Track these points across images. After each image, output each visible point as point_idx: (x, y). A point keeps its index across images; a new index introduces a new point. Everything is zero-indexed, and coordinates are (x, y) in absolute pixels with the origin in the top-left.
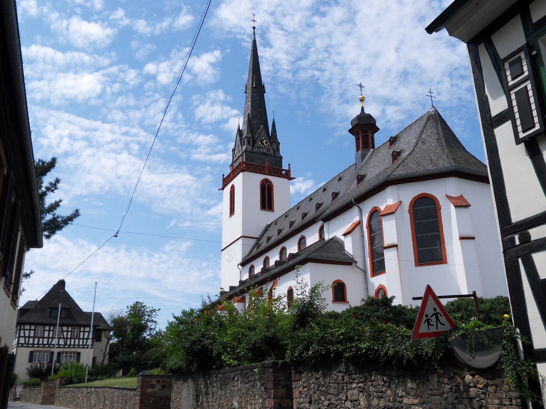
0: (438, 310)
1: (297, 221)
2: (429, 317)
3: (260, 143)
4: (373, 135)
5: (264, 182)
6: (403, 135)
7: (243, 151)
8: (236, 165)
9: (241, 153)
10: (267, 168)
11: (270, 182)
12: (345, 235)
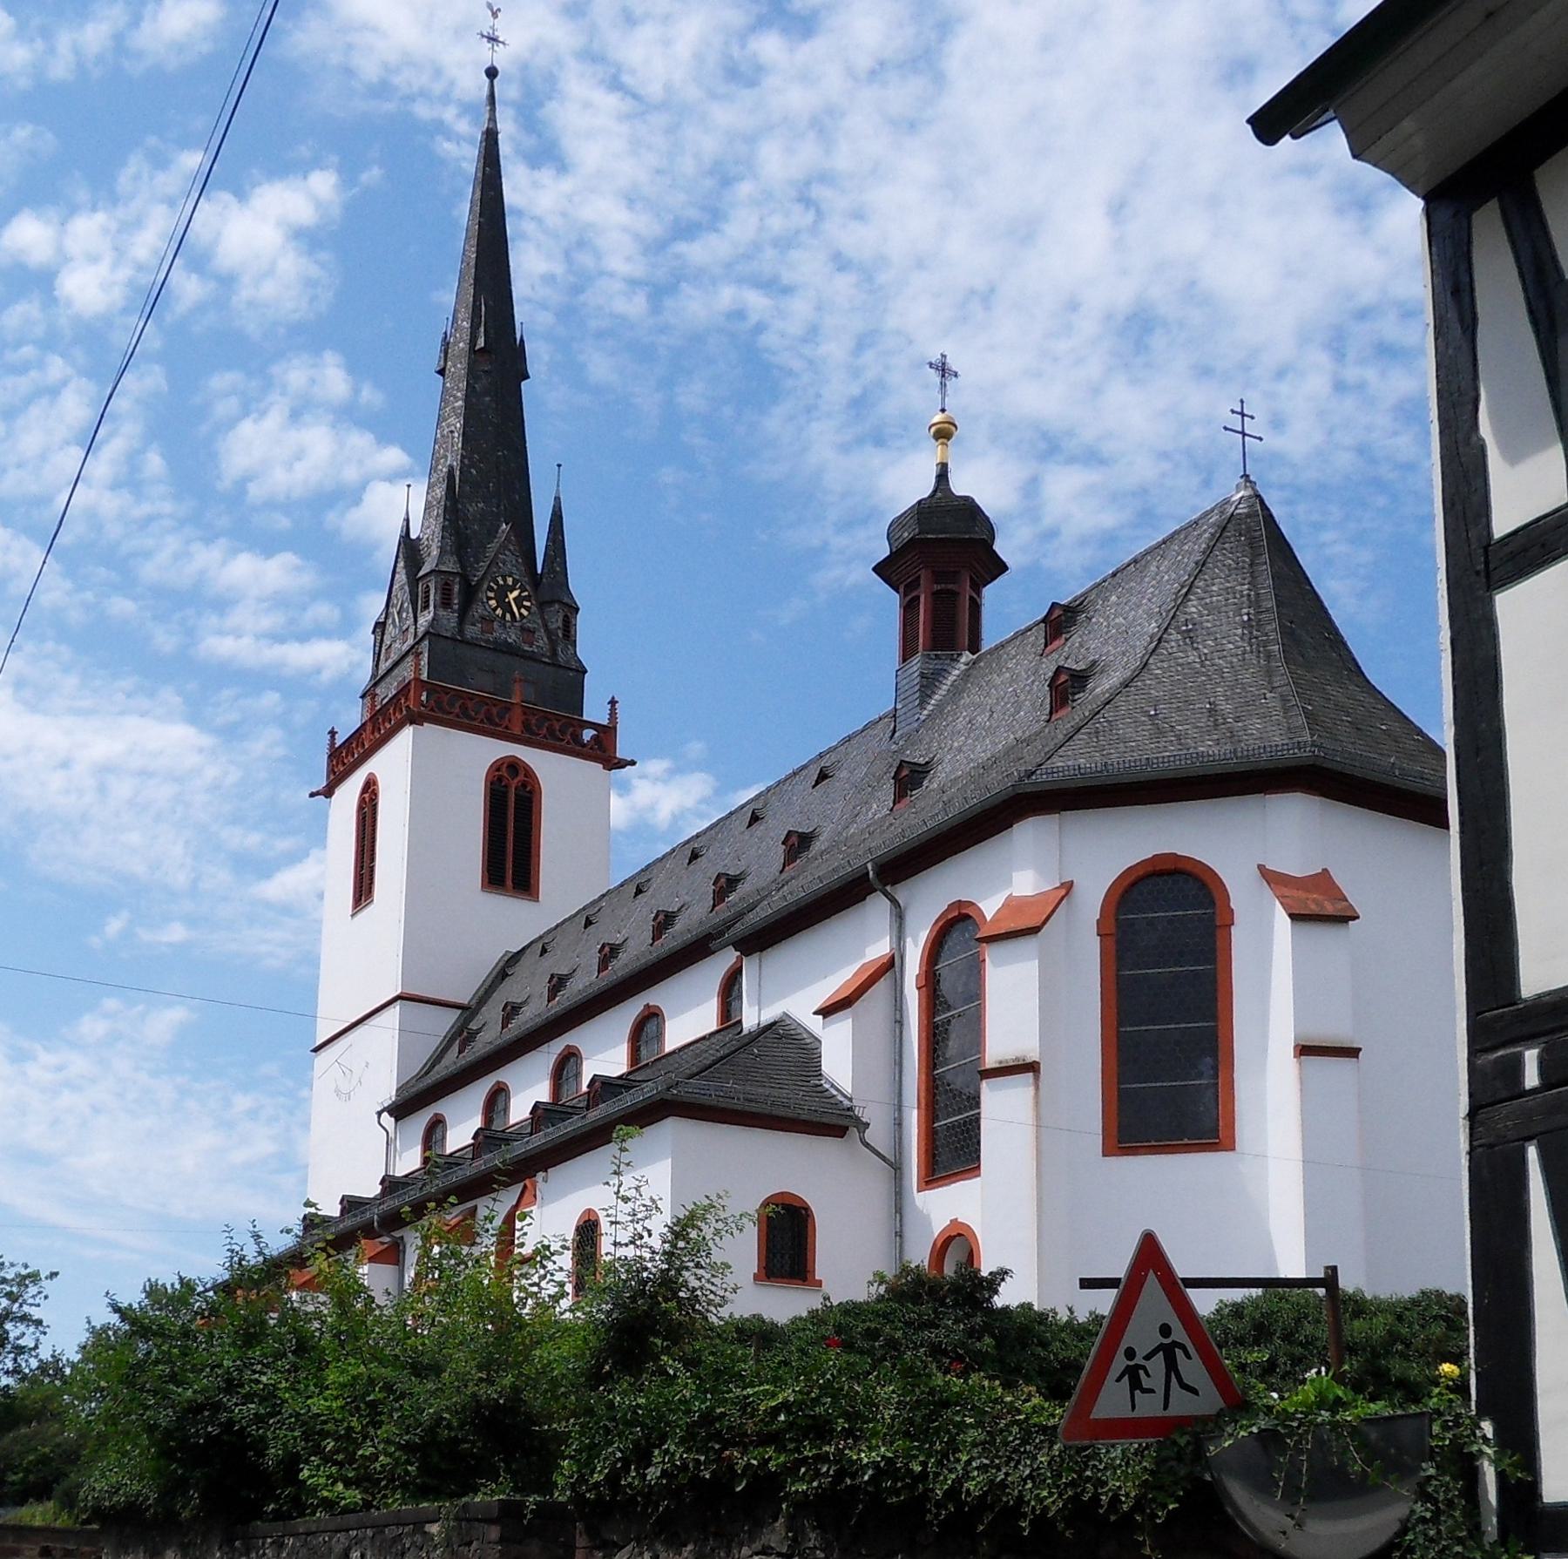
1: (630, 943)
2: (1139, 1360)
3: (493, 603)
4: (979, 593)
5: (504, 772)
6: (1106, 599)
8: (387, 691)
9: (410, 641)
11: (529, 773)
12: (827, 1011)
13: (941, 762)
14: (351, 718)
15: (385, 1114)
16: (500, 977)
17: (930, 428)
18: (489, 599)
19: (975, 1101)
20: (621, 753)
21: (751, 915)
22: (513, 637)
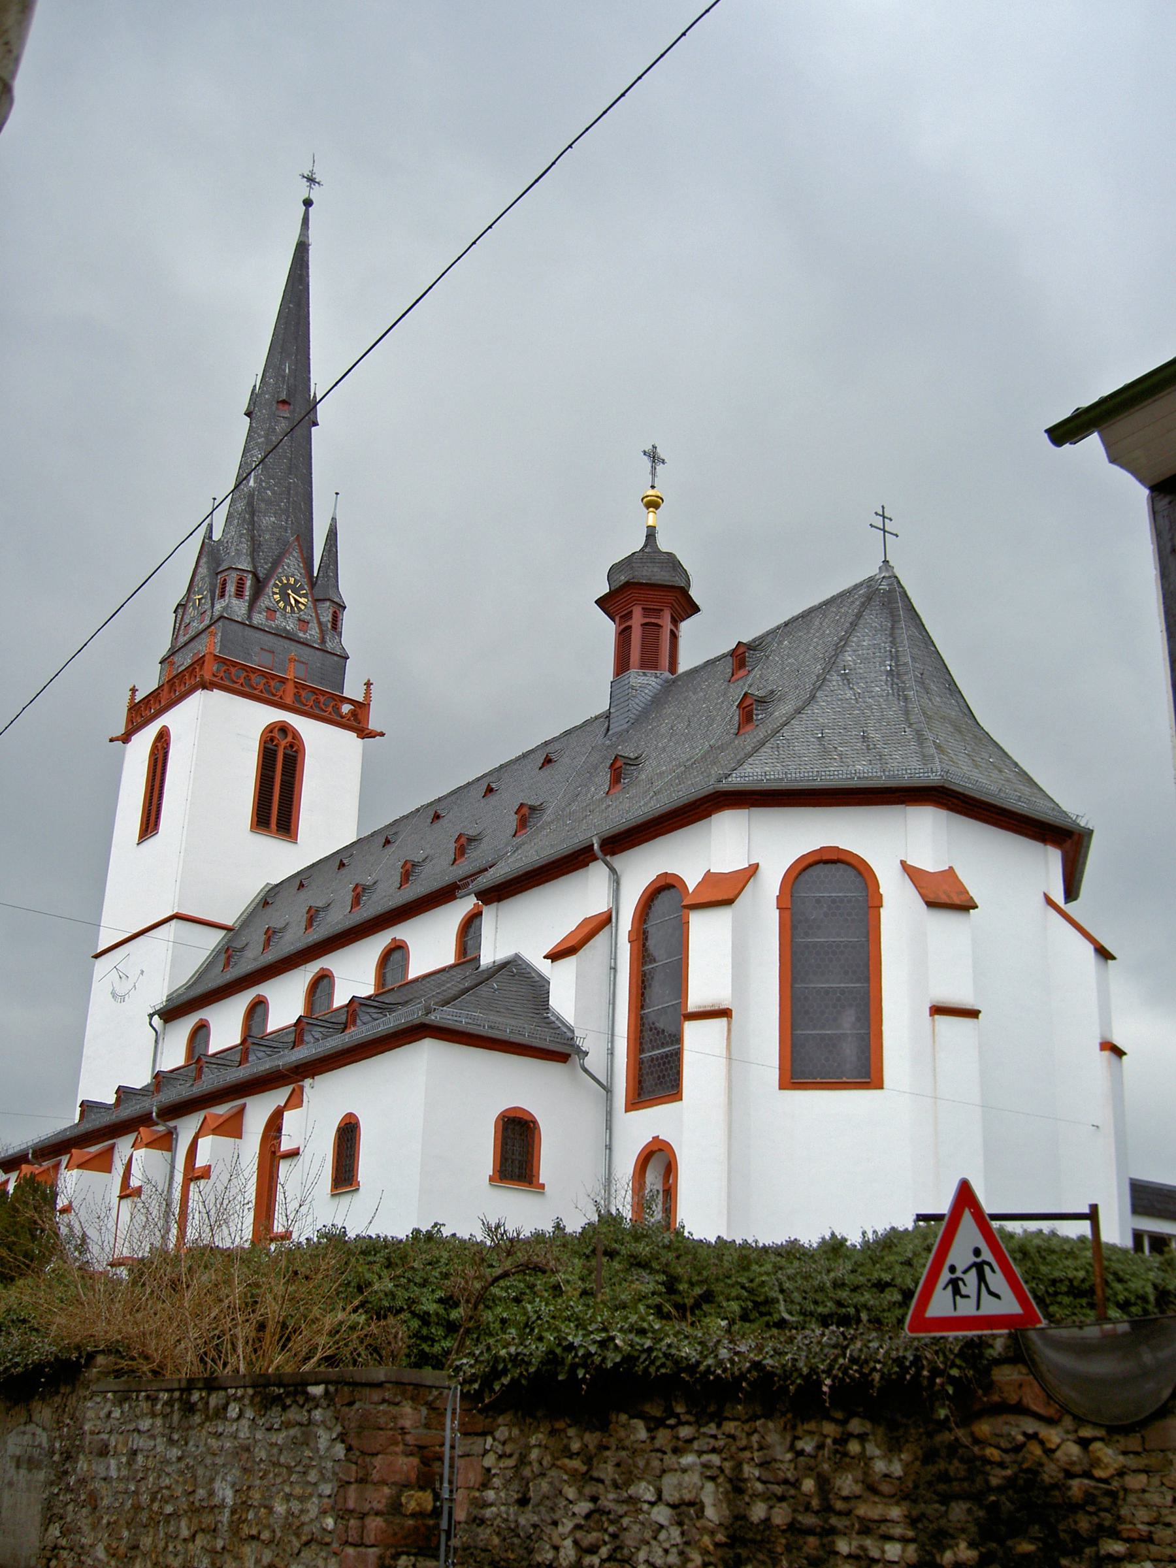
0: (987, 1255)
1: (380, 886)
2: (958, 1274)
3: (277, 597)
4: (676, 627)
5: (276, 734)
6: (781, 642)
7: (215, 618)
8: (185, 660)
9: (207, 622)
10: (290, 685)
11: (296, 736)
12: (555, 956)
13: (648, 757)
14: (148, 682)
15: (156, 1017)
16: (262, 905)
17: (642, 500)
18: (275, 593)
19: (678, 1039)
20: (373, 725)
21: (492, 871)
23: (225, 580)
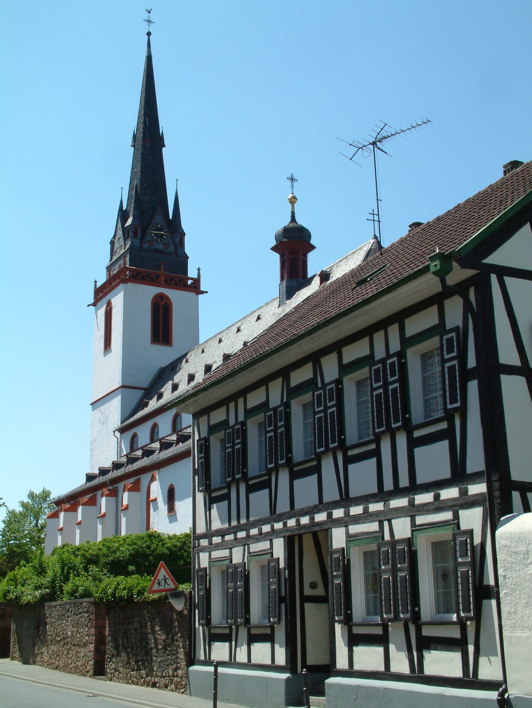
2: (160, 581)
8: (116, 270)
14: (102, 279)
22: (161, 247)
23: (129, 230)
